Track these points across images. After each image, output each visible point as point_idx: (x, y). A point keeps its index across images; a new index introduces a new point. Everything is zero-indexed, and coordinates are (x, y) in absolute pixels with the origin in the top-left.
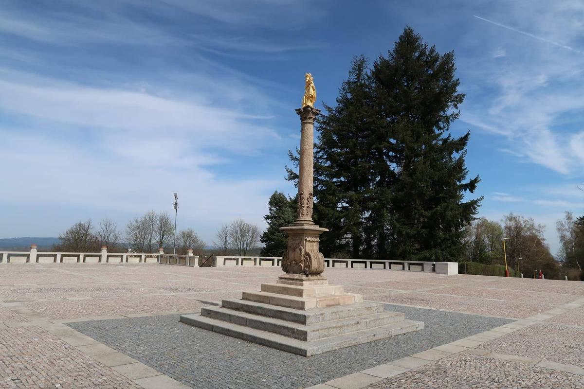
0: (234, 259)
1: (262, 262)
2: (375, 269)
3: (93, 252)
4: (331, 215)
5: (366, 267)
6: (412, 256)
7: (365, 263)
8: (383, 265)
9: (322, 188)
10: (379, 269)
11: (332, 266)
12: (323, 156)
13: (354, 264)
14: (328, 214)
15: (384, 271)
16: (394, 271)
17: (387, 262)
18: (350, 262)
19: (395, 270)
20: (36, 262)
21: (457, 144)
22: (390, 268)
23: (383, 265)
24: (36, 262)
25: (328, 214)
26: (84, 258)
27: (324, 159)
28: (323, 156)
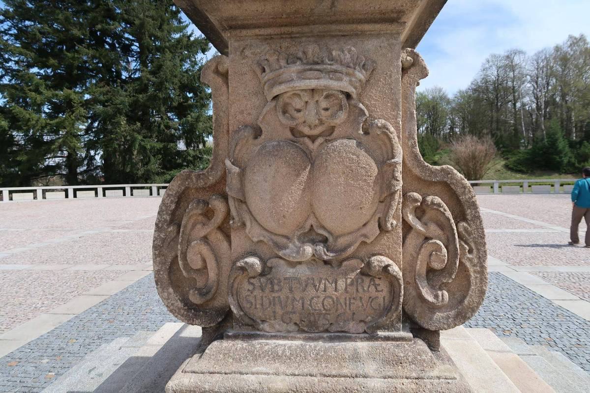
0: (147, 188)
1: (135, 191)
2: (111, 197)
3: (82, 185)
4: (34, 122)
5: (124, 194)
6: (157, 178)
7: (124, 189)
8: (122, 191)
9: (10, 81)
10: (116, 197)
11: (8, 198)
12: (10, 29)
13: (106, 191)
14: (29, 120)
15: (151, 199)
16: (139, 199)
17: (128, 187)
18: (41, 191)
19: (139, 196)
20: (74, 197)
21: (201, 42)
22: (132, 195)
23: (122, 191)
24: (74, 197)
25: (29, 120)
26: (132, 191)
27: (11, 35)
28: (10, 29)
